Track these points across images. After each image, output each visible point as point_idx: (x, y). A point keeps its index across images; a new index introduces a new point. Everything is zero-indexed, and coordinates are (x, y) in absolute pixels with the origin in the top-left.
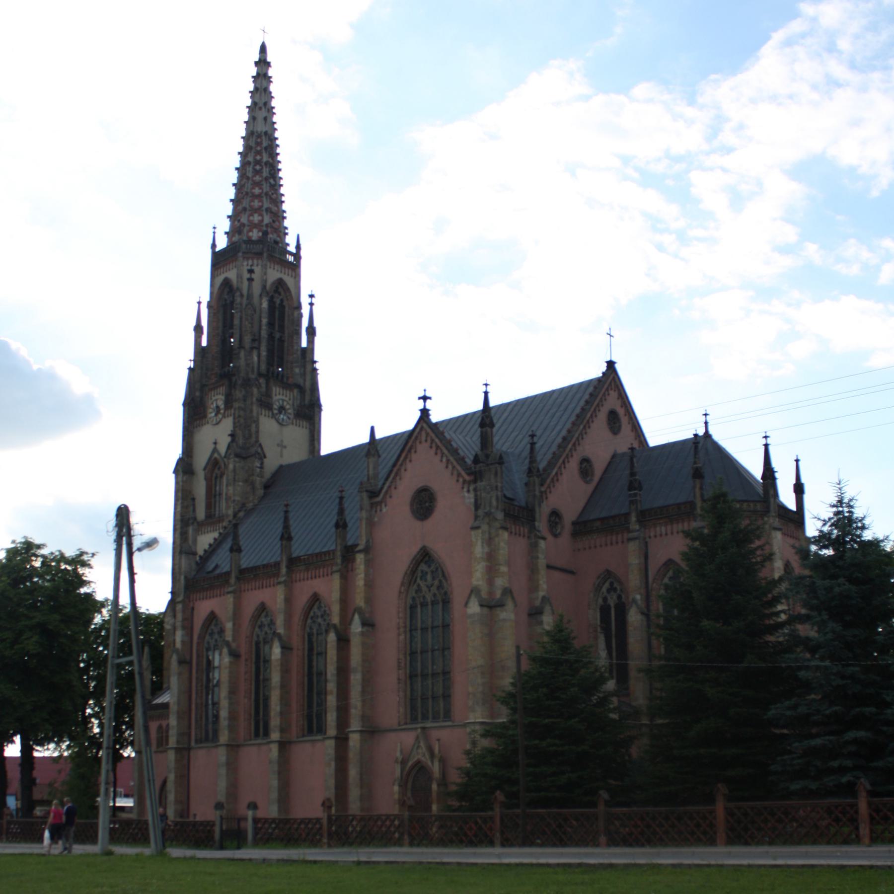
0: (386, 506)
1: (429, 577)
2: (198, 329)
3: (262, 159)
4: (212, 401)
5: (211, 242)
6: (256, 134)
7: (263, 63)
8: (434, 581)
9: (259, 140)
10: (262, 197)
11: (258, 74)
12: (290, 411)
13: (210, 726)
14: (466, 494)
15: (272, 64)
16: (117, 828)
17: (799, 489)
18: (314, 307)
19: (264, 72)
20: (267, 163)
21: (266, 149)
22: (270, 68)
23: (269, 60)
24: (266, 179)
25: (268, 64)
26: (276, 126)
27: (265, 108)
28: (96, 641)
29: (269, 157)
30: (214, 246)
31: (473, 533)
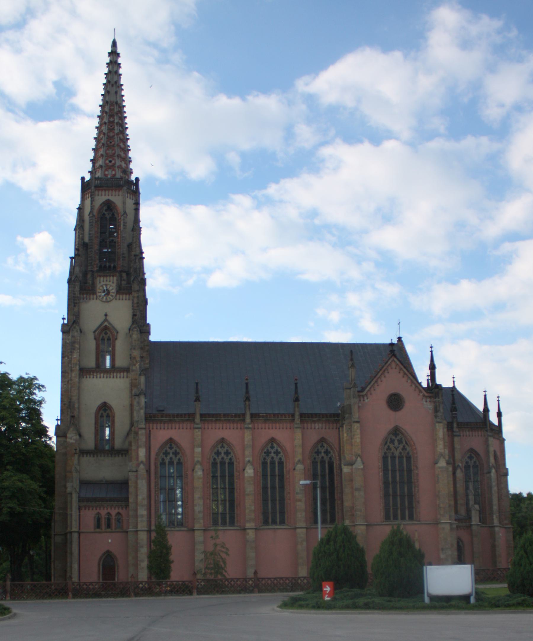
0: (367, 398)
1: (396, 443)
3: (114, 121)
6: (109, 103)
7: (114, 54)
8: (400, 445)
9: (112, 108)
10: (115, 147)
11: (111, 61)
14: (425, 403)
15: (121, 55)
17: (499, 414)
19: (115, 60)
20: (118, 123)
21: (117, 114)
22: (119, 58)
23: (118, 51)
24: (117, 134)
25: (118, 55)
26: (124, 98)
27: (116, 85)
29: (119, 120)
31: (437, 424)
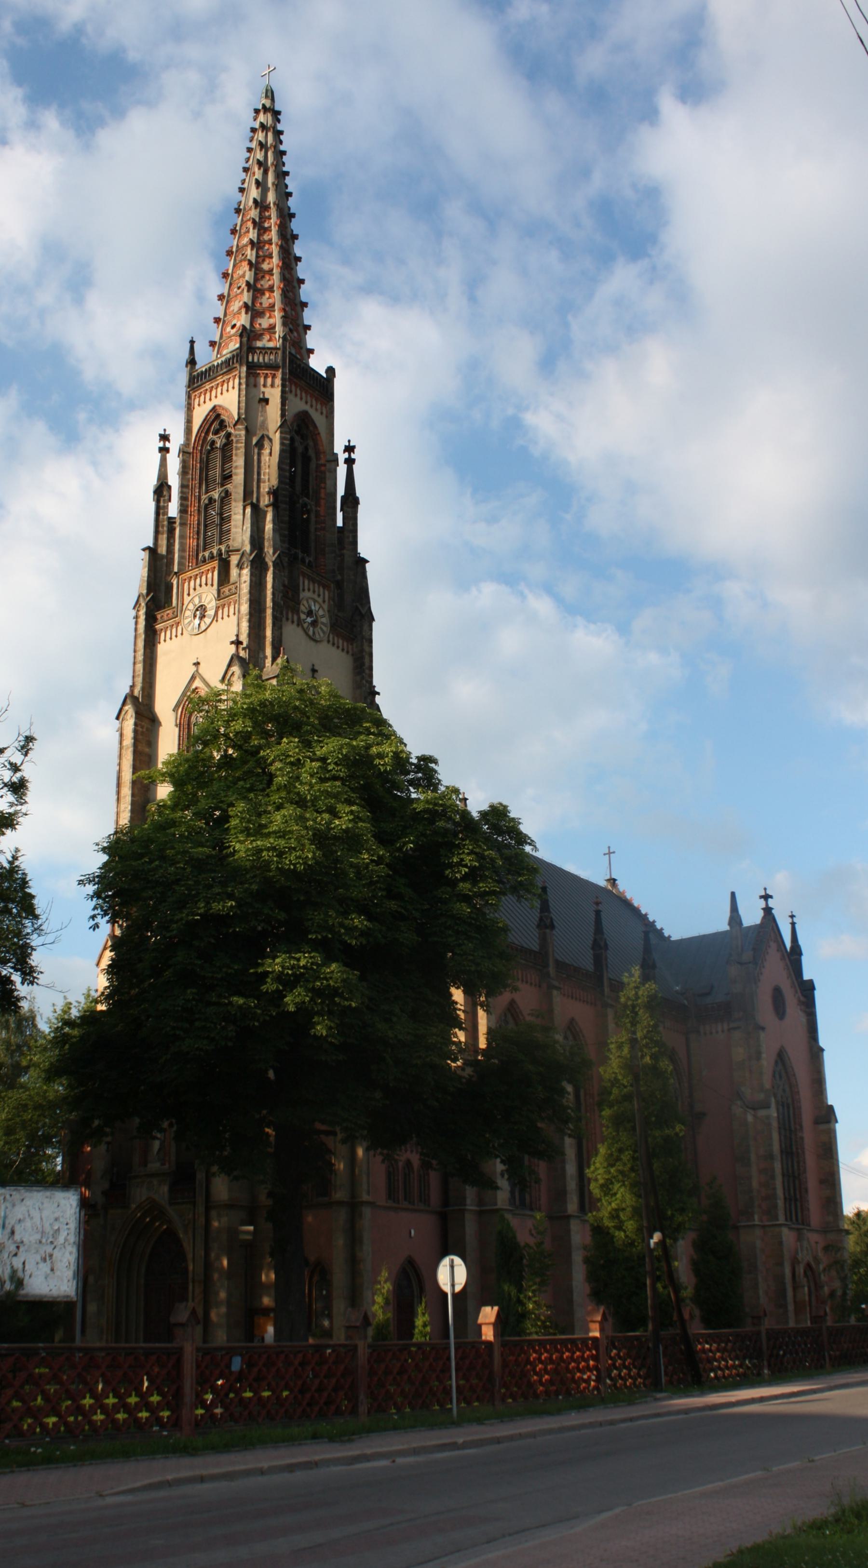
2: (161, 490)
4: (190, 598)
5: (186, 356)
12: (324, 620)
13: (203, 435)
16: (72, 1415)
18: (355, 467)
28: (465, 1049)
30: (192, 362)
